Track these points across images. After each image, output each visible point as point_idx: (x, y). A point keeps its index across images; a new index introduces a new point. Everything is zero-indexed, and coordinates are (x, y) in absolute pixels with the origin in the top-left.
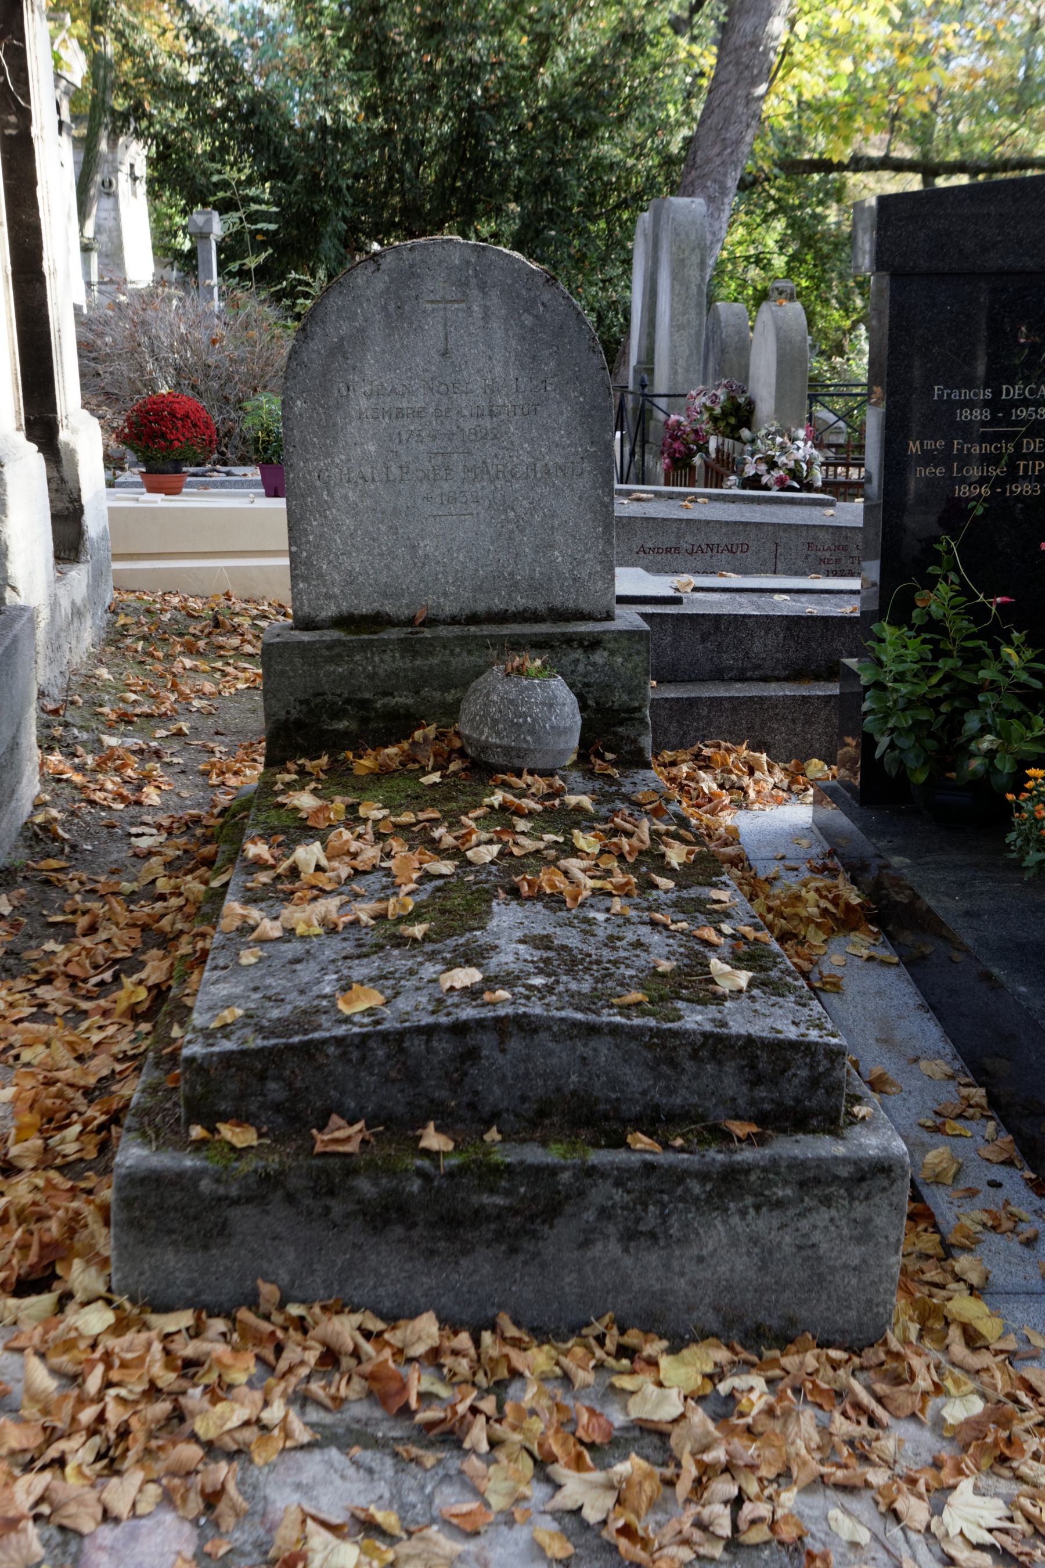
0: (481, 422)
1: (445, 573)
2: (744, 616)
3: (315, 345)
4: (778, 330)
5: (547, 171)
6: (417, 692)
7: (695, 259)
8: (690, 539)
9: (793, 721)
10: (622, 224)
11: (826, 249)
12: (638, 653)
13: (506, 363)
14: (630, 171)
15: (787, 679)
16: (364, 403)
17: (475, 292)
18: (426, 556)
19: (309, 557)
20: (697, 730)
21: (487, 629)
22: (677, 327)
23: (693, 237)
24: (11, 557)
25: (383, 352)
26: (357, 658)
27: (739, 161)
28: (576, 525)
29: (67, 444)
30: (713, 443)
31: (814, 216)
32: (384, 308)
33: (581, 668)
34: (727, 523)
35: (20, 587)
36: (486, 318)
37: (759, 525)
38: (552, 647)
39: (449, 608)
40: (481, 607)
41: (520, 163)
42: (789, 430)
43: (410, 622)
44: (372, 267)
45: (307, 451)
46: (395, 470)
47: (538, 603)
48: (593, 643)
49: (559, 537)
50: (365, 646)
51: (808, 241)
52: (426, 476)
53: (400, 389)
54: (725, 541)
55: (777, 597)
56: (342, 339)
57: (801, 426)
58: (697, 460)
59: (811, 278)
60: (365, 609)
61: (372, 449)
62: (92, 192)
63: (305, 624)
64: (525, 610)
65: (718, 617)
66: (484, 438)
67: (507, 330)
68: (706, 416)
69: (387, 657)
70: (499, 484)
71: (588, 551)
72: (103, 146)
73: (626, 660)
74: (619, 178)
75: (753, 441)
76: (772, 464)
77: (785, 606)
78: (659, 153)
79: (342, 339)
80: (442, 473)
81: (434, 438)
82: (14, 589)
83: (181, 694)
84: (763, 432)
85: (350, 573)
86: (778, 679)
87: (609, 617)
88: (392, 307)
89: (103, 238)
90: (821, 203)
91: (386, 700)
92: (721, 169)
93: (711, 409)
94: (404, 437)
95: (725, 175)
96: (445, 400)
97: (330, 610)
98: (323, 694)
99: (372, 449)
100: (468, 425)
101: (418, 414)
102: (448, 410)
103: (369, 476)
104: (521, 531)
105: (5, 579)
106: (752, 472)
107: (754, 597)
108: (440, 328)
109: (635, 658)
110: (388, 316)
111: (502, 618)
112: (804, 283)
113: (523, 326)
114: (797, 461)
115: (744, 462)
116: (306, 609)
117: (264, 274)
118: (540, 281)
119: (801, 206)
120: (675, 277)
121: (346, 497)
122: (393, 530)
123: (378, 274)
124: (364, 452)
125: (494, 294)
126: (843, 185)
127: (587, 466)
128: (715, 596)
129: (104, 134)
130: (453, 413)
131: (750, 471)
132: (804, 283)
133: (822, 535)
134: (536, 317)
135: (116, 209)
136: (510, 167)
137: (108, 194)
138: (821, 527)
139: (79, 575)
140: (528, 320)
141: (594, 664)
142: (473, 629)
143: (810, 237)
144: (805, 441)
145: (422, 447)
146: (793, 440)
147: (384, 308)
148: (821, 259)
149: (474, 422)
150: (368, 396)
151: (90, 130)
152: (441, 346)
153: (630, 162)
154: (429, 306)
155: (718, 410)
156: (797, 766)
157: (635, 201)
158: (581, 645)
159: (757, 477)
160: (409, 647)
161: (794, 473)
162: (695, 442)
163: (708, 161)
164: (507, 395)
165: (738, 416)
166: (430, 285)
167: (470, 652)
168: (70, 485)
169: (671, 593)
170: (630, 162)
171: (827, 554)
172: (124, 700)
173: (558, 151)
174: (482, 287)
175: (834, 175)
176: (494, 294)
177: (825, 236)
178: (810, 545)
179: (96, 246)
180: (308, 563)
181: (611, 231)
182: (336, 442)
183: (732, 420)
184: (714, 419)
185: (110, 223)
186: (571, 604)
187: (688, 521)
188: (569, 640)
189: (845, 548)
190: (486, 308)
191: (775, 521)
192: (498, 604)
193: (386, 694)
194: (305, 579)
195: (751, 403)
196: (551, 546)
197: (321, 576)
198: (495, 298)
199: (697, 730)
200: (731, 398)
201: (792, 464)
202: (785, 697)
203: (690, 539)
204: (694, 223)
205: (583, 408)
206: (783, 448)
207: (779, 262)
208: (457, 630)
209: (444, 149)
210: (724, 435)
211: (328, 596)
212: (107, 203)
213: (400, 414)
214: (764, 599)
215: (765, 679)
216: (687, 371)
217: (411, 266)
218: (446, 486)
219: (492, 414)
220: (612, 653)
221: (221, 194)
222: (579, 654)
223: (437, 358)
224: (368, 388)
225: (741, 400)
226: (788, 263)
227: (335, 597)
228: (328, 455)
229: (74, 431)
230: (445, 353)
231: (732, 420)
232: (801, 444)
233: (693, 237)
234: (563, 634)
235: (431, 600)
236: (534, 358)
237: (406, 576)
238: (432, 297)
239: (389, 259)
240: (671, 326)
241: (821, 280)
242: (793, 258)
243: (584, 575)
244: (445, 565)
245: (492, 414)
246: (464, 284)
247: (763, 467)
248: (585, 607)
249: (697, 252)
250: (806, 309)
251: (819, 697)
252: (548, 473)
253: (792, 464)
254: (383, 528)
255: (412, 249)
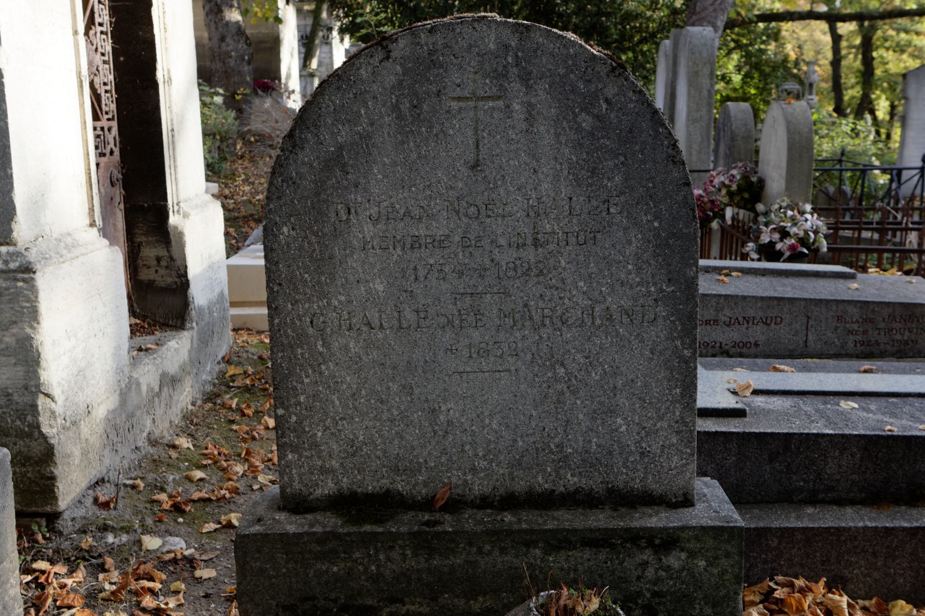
0: (522, 253)
1: (473, 444)
2: (817, 435)
3: (306, 156)
4: (788, 123)
5: (595, 19)
6: (434, 599)
7: (706, 71)
8: (728, 312)
9: (874, 554)
10: (643, 54)
11: (767, 70)
12: (728, 555)
13: (557, 177)
14: (649, 19)
15: (863, 503)
16: (369, 229)
17: (516, 86)
18: (450, 423)
19: (299, 422)
20: (765, 562)
21: (529, 520)
22: (691, 120)
23: (705, 55)
24: (43, 364)
25: (395, 164)
26: (357, 555)
27: (726, 8)
28: (646, 385)
29: (176, 228)
30: (729, 212)
31: (760, 50)
32: (396, 108)
33: (650, 573)
34: (762, 298)
35: (56, 392)
36: (530, 119)
37: (792, 300)
38: (612, 546)
39: (479, 486)
40: (520, 486)
41: (576, 14)
42: (797, 205)
43: (428, 504)
44: (380, 54)
45: (296, 290)
46: (409, 315)
47: (594, 482)
48: (667, 541)
49: (622, 400)
50: (367, 540)
51: (757, 66)
52: (450, 323)
53: (416, 212)
54: (760, 314)
55: (848, 405)
56: (341, 148)
57: (807, 201)
58: (715, 225)
59: (757, 88)
60: (371, 486)
61: (380, 288)
62: (317, 42)
63: (293, 503)
64: (577, 491)
65: (787, 438)
66: (526, 274)
67: (557, 135)
68: (724, 191)
69: (395, 555)
70: (544, 333)
71: (661, 418)
72: (324, 15)
73: (710, 564)
74: (641, 24)
75: (766, 214)
76: (784, 234)
77: (862, 420)
78: (668, 7)
79: (341, 148)
80: (471, 318)
81: (461, 274)
82: (48, 395)
83: (251, 466)
84: (776, 206)
85: (352, 443)
86: (853, 503)
87: (687, 501)
88: (405, 106)
89: (323, 69)
90: (763, 42)
91: (394, 608)
92: (714, 14)
93: (730, 186)
94: (422, 273)
95: (716, 18)
96: (475, 225)
97: (327, 487)
98: (314, 598)
99: (380, 288)
100: (506, 257)
101: (440, 243)
102: (479, 239)
103: (376, 322)
104: (573, 393)
105: (38, 386)
106: (767, 240)
107: (818, 402)
108: (470, 132)
109: (723, 561)
110: (400, 117)
111: (546, 501)
112: (753, 91)
113: (579, 129)
114: (806, 232)
115: (760, 232)
116: (297, 485)
117: (305, 76)
118: (603, 70)
119: (751, 44)
120: (691, 84)
121: (346, 348)
122: (407, 389)
123: (387, 64)
124: (369, 292)
125: (542, 87)
126: (779, 31)
127: (662, 311)
128: (777, 403)
129: (325, 7)
130: (486, 242)
131: (765, 239)
132: (753, 91)
133: (851, 309)
134: (597, 117)
135: (331, 52)
136: (569, 16)
137: (327, 43)
138: (850, 302)
139: (177, 348)
140: (586, 122)
141: (668, 569)
142: (508, 517)
143: (757, 64)
144: (812, 214)
145: (444, 286)
146: (802, 213)
147: (396, 108)
148: (764, 76)
149: (513, 254)
150: (375, 221)
151: (317, 6)
152: (471, 157)
153: (649, 13)
154: (455, 105)
155: (734, 187)
156: (878, 604)
157: (652, 38)
158: (650, 543)
159: (772, 244)
160: (424, 542)
161: (803, 241)
162: (712, 210)
163: (705, 9)
164: (557, 219)
165: (751, 192)
166: (456, 77)
167: (503, 551)
168: (178, 263)
169: (729, 402)
170: (649, 13)
171: (855, 326)
172: (189, 479)
173: (602, 6)
174: (525, 79)
175: (773, 24)
176: (542, 87)
177: (767, 62)
178: (839, 318)
179: (317, 74)
180: (298, 429)
181: (636, 58)
182: (333, 279)
183: (746, 195)
184: (730, 194)
185: (327, 61)
186: (637, 484)
187: (726, 296)
188: (635, 537)
189: (872, 321)
190: (530, 107)
191: (806, 296)
192: (542, 483)
193: (393, 600)
194: (295, 449)
195: (761, 182)
196: (612, 412)
197: (315, 445)
198: (542, 94)
199: (765, 562)
200: (745, 177)
201: (802, 234)
202: (866, 528)
203: (728, 312)
204: (705, 44)
205: (657, 236)
206: (793, 219)
207: (737, 79)
208: (486, 516)
209: (526, 6)
210: (739, 207)
211: (324, 471)
212: (325, 48)
213: (416, 244)
214: (830, 407)
215: (840, 502)
216: (700, 153)
217: (431, 53)
218: (476, 335)
219: (536, 244)
220: (692, 555)
221: (364, 31)
222: (647, 555)
223: (465, 171)
224: (374, 211)
225: (754, 179)
226: (742, 79)
227: (332, 471)
228: (322, 295)
229: (186, 216)
230: (475, 166)
231: (746, 195)
232: (809, 216)
233: (705, 55)
234: (628, 530)
235: (455, 477)
236: (593, 171)
237: (423, 446)
238: (458, 92)
239: (402, 43)
240: (688, 120)
241: (764, 89)
242: (746, 76)
243: (656, 449)
244: (473, 434)
245: (536, 244)
246: (500, 76)
247: (777, 236)
248: (656, 488)
249: (708, 65)
250: (753, 107)
251: (904, 529)
252: (610, 319)
253: (802, 234)
254: (394, 387)
255: (432, 30)
